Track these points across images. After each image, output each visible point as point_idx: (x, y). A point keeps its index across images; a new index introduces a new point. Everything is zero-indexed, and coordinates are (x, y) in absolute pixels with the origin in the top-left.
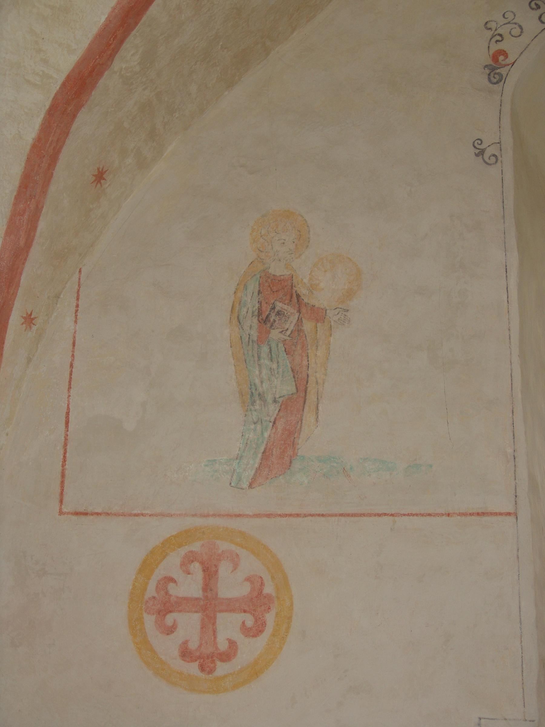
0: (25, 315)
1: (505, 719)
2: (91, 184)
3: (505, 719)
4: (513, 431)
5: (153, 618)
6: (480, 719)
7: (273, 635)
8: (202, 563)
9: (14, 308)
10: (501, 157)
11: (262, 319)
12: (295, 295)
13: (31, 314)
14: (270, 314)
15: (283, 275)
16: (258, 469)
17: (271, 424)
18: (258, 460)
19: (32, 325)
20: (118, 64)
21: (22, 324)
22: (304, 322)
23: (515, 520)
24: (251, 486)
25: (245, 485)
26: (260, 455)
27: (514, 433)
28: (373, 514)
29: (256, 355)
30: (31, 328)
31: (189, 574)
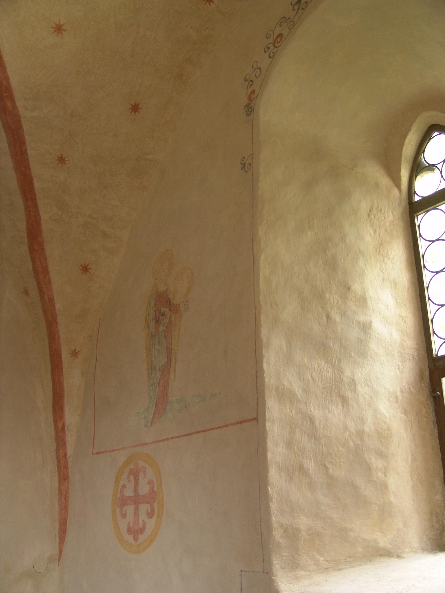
0: (71, 352)
1: (253, 572)
2: (81, 274)
3: (253, 572)
4: (256, 358)
5: (119, 509)
6: (241, 571)
7: (158, 517)
8: (134, 475)
9: (62, 351)
10: (253, 163)
11: (156, 321)
12: (168, 301)
13: (75, 350)
14: (159, 316)
15: (164, 290)
16: (154, 414)
17: (158, 384)
18: (154, 408)
19: (78, 356)
20: (44, 216)
21: (71, 357)
22: (172, 315)
23: (257, 423)
24: (151, 425)
25: (149, 425)
26: (155, 404)
27: (256, 359)
28: (196, 432)
29: (153, 344)
30: (77, 357)
31: (130, 482)
